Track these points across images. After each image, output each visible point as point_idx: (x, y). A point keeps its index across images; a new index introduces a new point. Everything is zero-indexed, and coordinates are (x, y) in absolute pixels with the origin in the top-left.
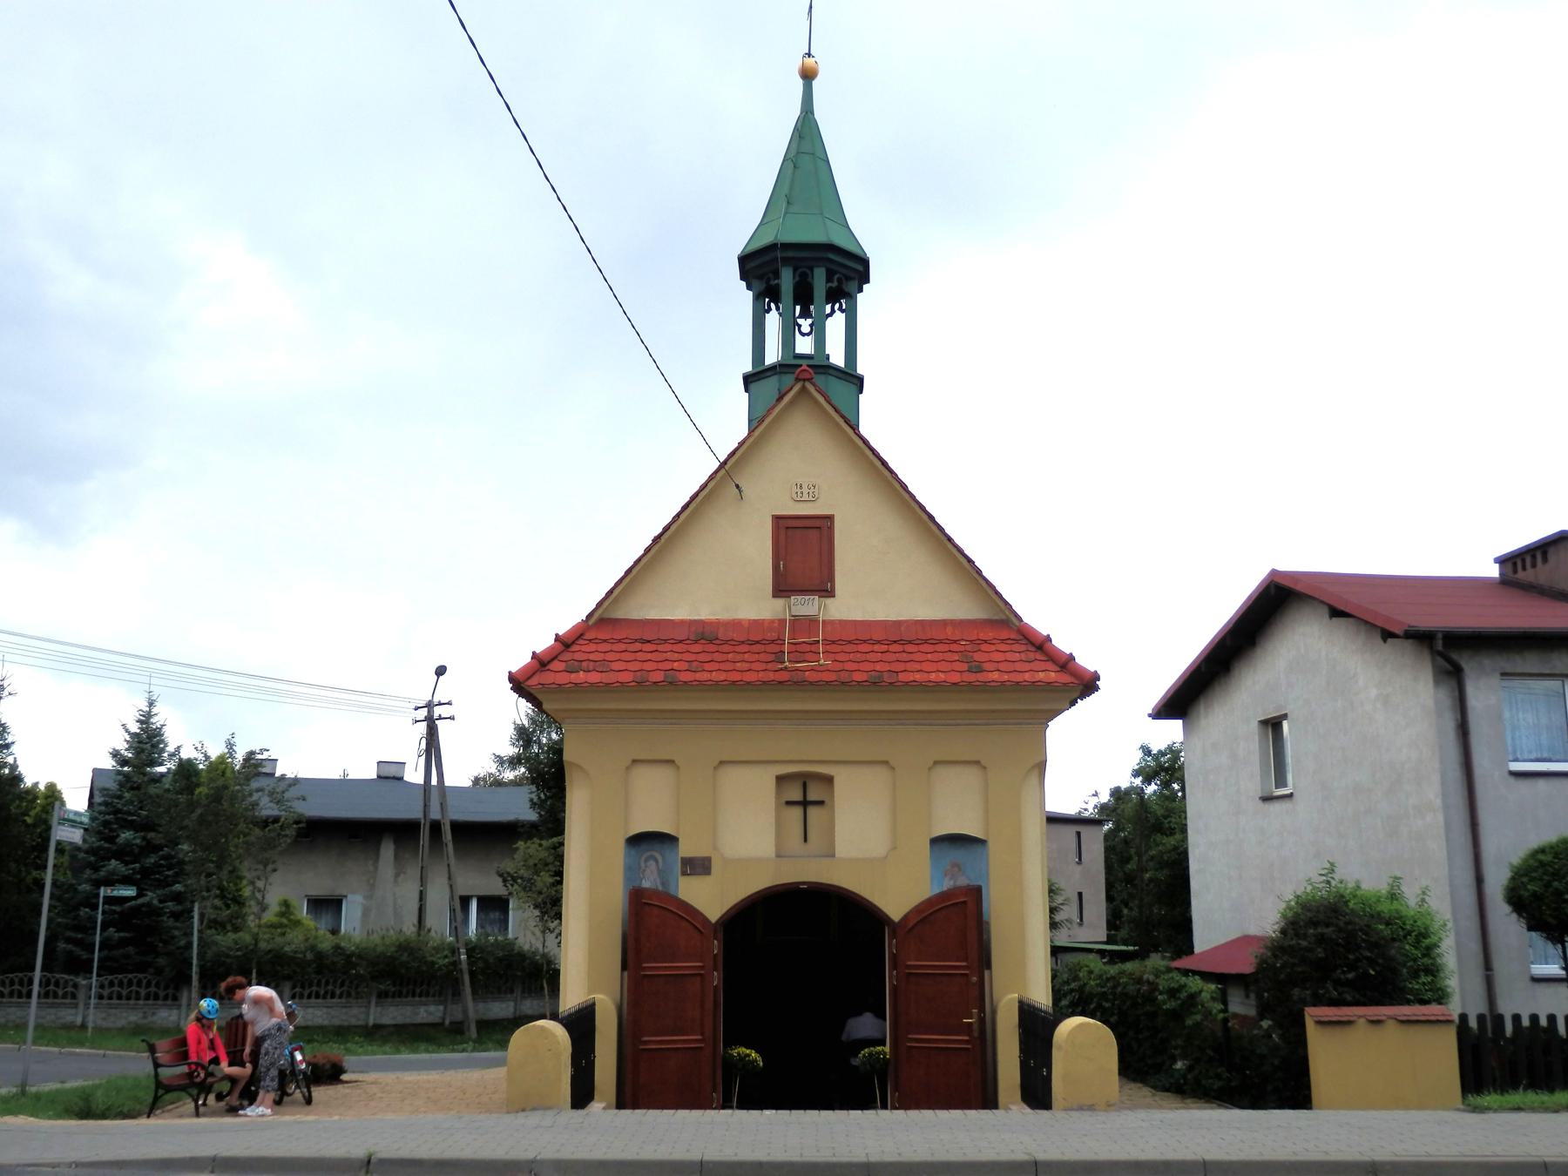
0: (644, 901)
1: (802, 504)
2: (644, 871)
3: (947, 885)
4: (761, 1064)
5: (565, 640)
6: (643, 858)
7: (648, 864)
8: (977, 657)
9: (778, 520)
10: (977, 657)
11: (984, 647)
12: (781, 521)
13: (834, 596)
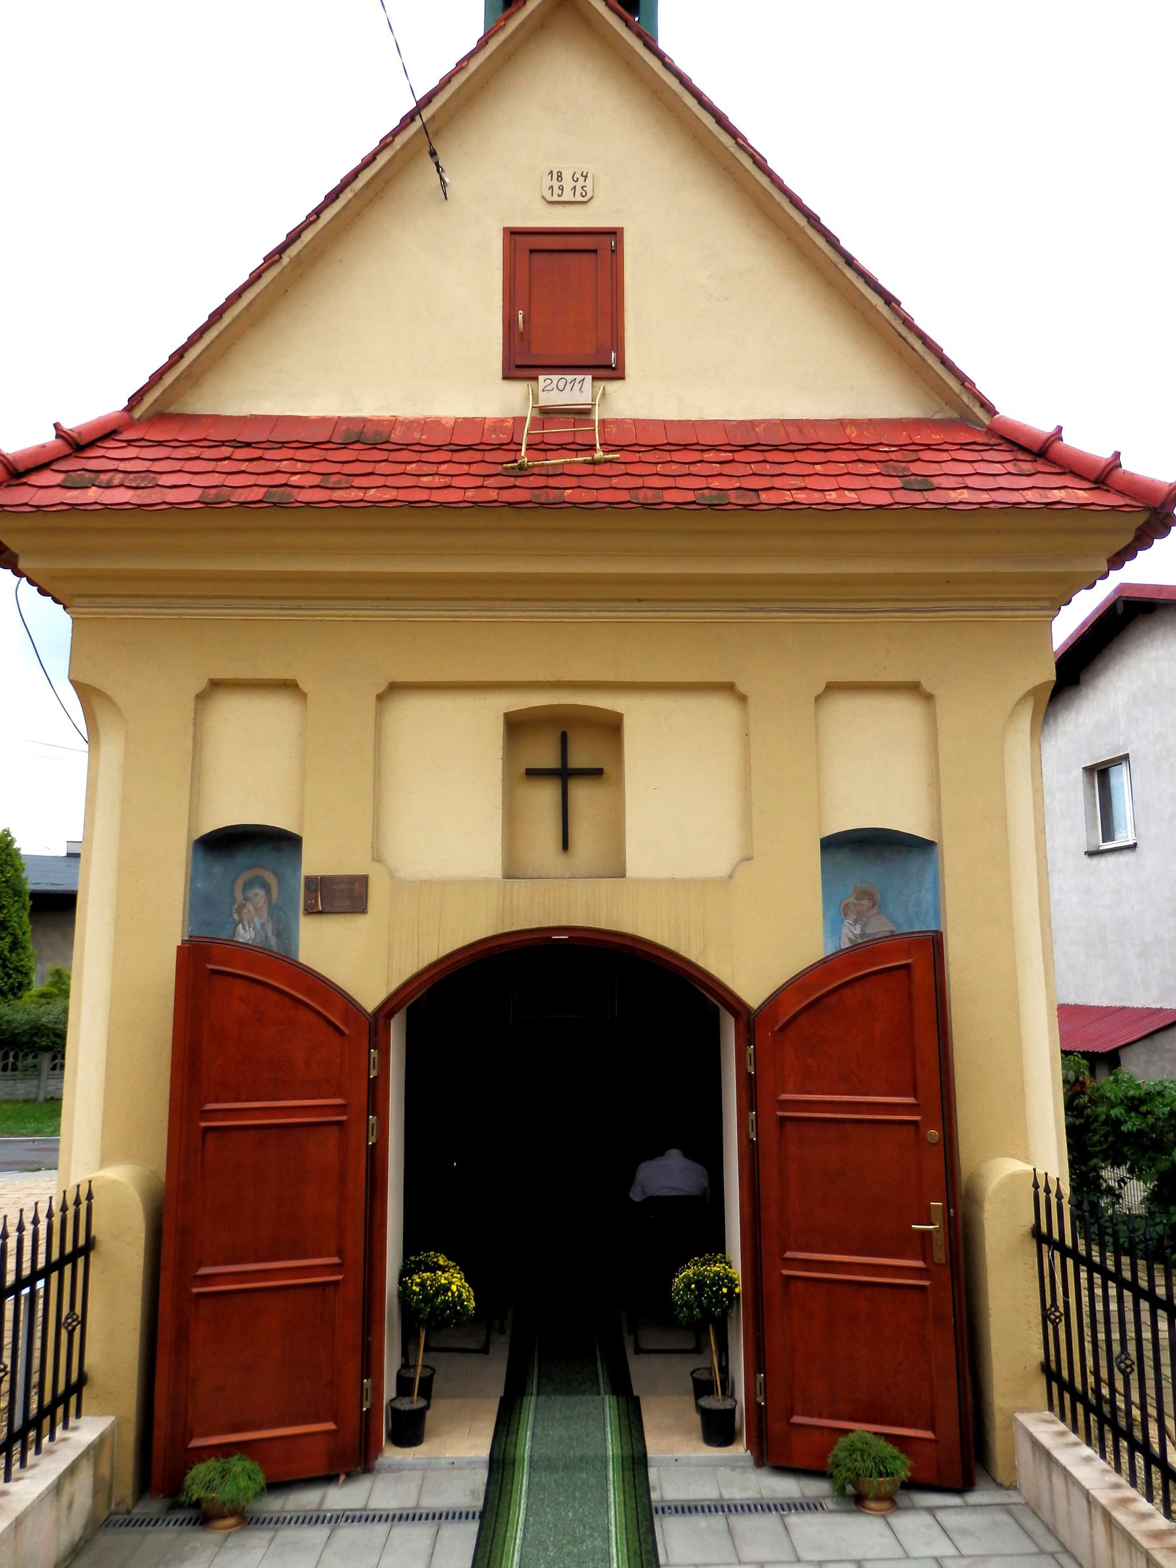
0: (210, 966)
1: (559, 210)
2: (242, 907)
3: (850, 933)
4: (472, 1304)
6: (240, 882)
7: (251, 893)
8: (916, 468)
9: (512, 234)
10: (916, 468)
11: (927, 455)
12: (518, 238)
13: (622, 378)
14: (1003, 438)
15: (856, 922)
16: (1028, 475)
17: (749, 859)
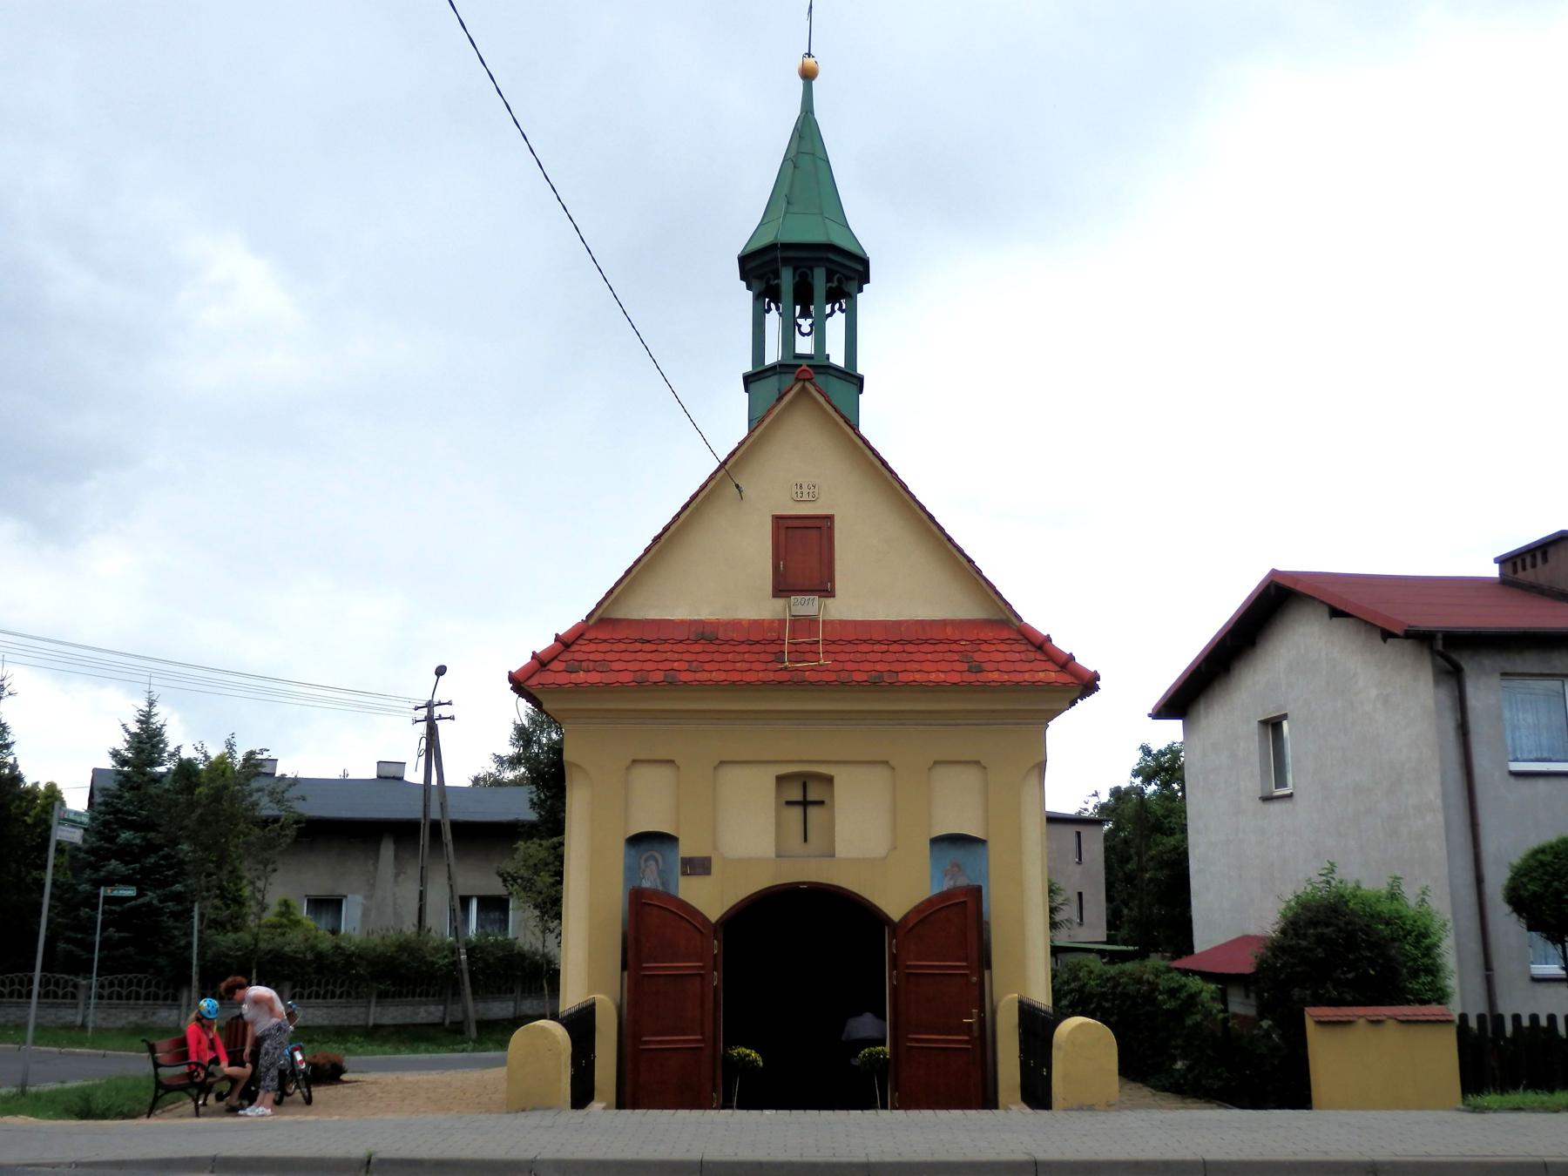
0: (644, 901)
1: (803, 505)
2: (644, 871)
3: (947, 884)
5: (566, 640)
6: (643, 858)
7: (648, 864)
8: (977, 656)
10: (977, 656)
11: (984, 647)
12: (781, 522)
13: (834, 596)
14: (1023, 635)
15: (951, 879)
16: (1030, 662)
17: (895, 848)
